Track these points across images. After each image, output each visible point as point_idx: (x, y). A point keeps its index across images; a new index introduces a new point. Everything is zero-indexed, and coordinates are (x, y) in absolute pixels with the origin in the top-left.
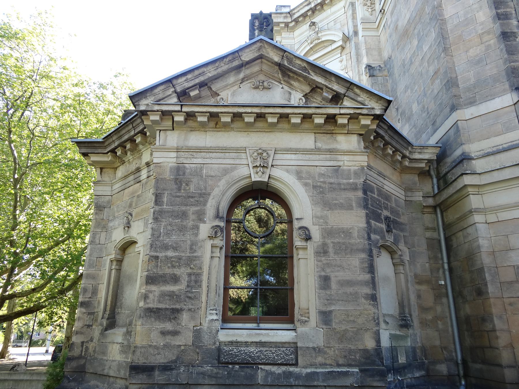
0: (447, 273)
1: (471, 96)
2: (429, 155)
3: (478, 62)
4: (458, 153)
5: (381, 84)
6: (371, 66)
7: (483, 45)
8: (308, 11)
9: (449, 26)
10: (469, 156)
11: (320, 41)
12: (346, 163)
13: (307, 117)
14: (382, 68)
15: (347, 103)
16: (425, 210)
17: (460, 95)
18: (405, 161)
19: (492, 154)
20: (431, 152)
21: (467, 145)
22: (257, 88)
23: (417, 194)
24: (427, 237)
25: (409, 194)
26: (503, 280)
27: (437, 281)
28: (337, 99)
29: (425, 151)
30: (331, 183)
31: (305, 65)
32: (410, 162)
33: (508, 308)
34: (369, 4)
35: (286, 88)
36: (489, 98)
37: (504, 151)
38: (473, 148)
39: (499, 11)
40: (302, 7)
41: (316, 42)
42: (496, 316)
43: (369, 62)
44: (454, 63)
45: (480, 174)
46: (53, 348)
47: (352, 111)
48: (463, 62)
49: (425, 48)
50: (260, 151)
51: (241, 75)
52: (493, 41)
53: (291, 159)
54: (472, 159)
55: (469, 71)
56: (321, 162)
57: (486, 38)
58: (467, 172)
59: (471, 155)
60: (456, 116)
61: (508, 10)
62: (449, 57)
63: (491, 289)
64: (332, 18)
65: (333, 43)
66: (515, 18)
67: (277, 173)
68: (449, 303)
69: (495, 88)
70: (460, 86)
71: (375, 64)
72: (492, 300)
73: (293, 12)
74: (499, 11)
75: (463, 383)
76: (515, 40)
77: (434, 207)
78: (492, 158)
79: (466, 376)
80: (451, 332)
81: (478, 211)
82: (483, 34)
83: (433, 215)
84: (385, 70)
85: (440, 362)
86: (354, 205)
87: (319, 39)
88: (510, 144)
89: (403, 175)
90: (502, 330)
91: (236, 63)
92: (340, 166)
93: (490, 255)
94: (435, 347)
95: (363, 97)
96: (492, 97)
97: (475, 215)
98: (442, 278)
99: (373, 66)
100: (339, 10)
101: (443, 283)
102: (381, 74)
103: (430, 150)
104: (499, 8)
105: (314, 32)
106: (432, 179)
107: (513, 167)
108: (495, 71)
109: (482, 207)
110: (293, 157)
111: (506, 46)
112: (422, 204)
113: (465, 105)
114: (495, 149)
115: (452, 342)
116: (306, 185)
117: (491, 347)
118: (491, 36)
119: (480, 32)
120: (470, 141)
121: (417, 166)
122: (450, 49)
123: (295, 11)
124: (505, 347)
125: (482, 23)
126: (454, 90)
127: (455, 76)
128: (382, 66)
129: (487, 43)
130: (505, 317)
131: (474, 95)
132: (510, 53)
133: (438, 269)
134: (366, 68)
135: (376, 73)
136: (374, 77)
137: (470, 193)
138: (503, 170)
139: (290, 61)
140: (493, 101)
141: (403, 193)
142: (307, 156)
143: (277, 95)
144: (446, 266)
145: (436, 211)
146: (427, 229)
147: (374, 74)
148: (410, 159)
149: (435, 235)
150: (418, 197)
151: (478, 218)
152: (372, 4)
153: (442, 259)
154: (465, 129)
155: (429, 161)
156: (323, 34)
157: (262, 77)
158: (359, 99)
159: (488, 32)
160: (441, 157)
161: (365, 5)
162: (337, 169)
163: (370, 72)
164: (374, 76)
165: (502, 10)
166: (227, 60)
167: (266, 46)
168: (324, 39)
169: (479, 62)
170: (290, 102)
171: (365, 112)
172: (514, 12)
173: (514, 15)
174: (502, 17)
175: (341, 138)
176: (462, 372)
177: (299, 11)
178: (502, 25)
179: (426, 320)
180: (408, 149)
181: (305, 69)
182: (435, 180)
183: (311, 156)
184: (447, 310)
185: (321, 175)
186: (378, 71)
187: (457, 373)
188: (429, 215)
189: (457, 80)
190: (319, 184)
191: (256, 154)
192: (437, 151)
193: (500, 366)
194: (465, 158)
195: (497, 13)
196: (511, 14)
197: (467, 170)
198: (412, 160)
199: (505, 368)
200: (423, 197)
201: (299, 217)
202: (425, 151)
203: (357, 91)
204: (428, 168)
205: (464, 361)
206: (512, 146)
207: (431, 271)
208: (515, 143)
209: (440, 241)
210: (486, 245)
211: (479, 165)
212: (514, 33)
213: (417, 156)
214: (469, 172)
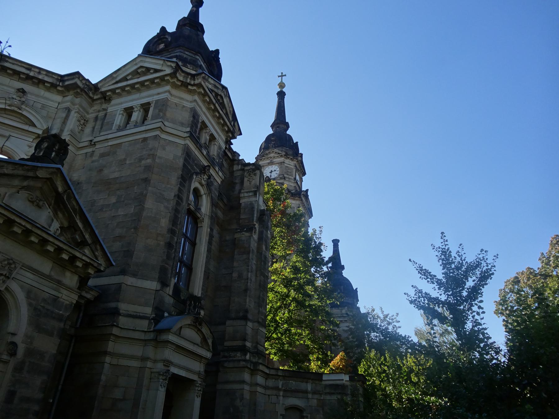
4: (113, 305)
8: (24, 73)
9: (144, 214)
11: (20, 111)
12: (64, 297)
13: (59, 250)
15: (87, 251)
22: (32, 202)
28: (82, 244)
30: (48, 310)
31: (77, 207)
34: (82, 123)
35: (51, 214)
38: (123, 307)
40: (20, 64)
41: (16, 109)
45: (121, 328)
47: (88, 261)
49: (121, 212)
50: (11, 262)
51: (25, 183)
53: (29, 278)
56: (48, 289)
64: (43, 101)
65: (32, 126)
67: (14, 286)
73: (7, 59)
81: (112, 354)
86: (55, 333)
87: (20, 109)
91: (30, 174)
92: (59, 297)
95: (99, 253)
96: (144, 277)
100: (52, 101)
105: (19, 99)
110: (32, 276)
114: (135, 314)
116: (30, 305)
123: (10, 61)
139: (69, 198)
142: (41, 280)
143: (43, 216)
152: (84, 124)
156: (27, 108)
157: (38, 193)
158: (97, 253)
161: (79, 121)
162: (56, 299)
166: (27, 168)
167: (59, 175)
168: (24, 113)
170: (50, 227)
171: (96, 265)
175: (68, 274)
177: (13, 64)
181: (75, 210)
182: (81, 315)
183: (43, 281)
185: (44, 300)
190: (39, 307)
191: (6, 262)
192: (96, 294)
194: (116, 312)
201: (12, 331)
203: (98, 247)
211: (122, 321)
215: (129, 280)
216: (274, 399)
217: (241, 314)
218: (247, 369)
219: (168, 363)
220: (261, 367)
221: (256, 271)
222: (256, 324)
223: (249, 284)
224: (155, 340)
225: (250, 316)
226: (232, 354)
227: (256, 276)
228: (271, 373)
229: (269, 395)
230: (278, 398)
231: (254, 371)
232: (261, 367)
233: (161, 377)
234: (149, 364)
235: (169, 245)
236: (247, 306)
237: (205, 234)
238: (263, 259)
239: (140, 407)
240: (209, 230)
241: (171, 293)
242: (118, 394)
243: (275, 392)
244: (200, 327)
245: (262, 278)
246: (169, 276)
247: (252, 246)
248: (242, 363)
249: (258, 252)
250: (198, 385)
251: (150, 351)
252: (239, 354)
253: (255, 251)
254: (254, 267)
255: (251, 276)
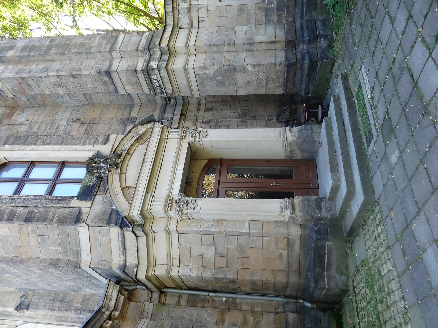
0: (217, 294)
1: (72, 252)
2: (114, 291)
3: (43, 241)
5: (40, 299)
6: (18, 306)
7: (30, 235)
10: (122, 266)
14: (24, 295)
16: (162, 301)
17: (68, 260)
18: (114, 315)
19: (125, 250)
20: (112, 289)
21: (113, 264)
23: (147, 306)
24: (185, 305)
25: (145, 315)
26: (224, 265)
27: (223, 304)
29: (110, 294)
32: (117, 310)
33: (245, 266)
36: (77, 240)
37: (124, 242)
39: (5, 218)
42: (252, 277)
43: (14, 306)
44: (37, 258)
45: (139, 263)
46: (255, 239)
48: (39, 251)
49: (17, 271)
52: (29, 227)
54: (125, 264)
55: (49, 249)
57: (25, 231)
58: (135, 271)
59: (121, 264)
60: (85, 266)
61: (7, 211)
62: (30, 260)
63: (231, 276)
66: (17, 208)
68: (241, 298)
69: (70, 235)
70: (60, 258)
71: (17, 301)
72: (239, 278)
74: (5, 218)
75: (301, 301)
76: (36, 213)
77: (161, 292)
78: (128, 251)
79: (296, 298)
80: (264, 301)
81: (169, 271)
82: (20, 232)
83: (168, 295)
84: (27, 293)
85: (286, 318)
88: (120, 237)
89: (127, 317)
90: (262, 275)
93: (204, 270)
94: (275, 320)
97: (172, 275)
98: (221, 298)
99: (18, 303)
101: (224, 299)
102: (30, 298)
103: (110, 290)
104: (3, 217)
106: (136, 289)
107: (138, 241)
108: (56, 232)
109: (166, 266)
111: (37, 221)
112: (156, 304)
113: (78, 258)
114: (121, 247)
115: (271, 302)
117: (275, 284)
118: (24, 228)
119: (17, 234)
120: (110, 262)
121: (121, 304)
122: (24, 258)
124: (274, 276)
125: (11, 231)
126: (61, 264)
127: (49, 260)
128: (22, 294)
129: (30, 232)
130: (252, 270)
131: (71, 250)
132: (44, 220)
133: (213, 300)
134: (18, 311)
135: (26, 302)
136: (30, 305)
137: (153, 274)
138: (139, 248)
140: (81, 239)
141: (143, 320)
144: (211, 294)
145: (165, 292)
146: (178, 302)
147: (27, 304)
148: (113, 310)
149: (185, 297)
150: (149, 307)
151: (174, 273)
153: (205, 296)
154: (99, 263)
155: (120, 292)
159: (20, 229)
160: (118, 281)
163: (24, 309)
164: (29, 305)
165: (5, 216)
169: (44, 241)
172: (11, 208)
173: (14, 208)
174: (11, 218)
176: (293, 300)
178: (18, 220)
179: (254, 323)
180: (103, 313)
184: (246, 300)
186: (26, 300)
187: (294, 304)
188: (167, 298)
189: (54, 259)
193: (287, 283)
194: (123, 268)
195: (5, 221)
196: (12, 210)
197: (134, 271)
198: (115, 308)
199: (289, 280)
200: (150, 302)
202: (110, 294)
204: (126, 293)
205: (286, 297)
206: (121, 236)
207: (214, 307)
208: (120, 233)
209: (190, 295)
210: (197, 271)
211: (131, 260)
212: (29, 212)
213: (112, 303)
214: (136, 270)
215: (85, 257)
216: (203, 14)
217: (106, 78)
218: (169, 67)
219: (169, 203)
220: (164, 44)
221: (46, 61)
222: (115, 54)
223: (63, 73)
224: (142, 226)
225: (104, 68)
226: (156, 84)
227: (53, 60)
228: (172, 23)
229: (199, 21)
230: (201, 8)
231: (171, 53)
232: (164, 44)
233: (185, 212)
234: (172, 227)
235: (28, 219)
236: (93, 72)
237: (13, 152)
238: (26, 53)
239: (219, 230)
240: (7, 147)
241: (89, 204)
242: (209, 253)
243: (194, 14)
244: (124, 153)
245: (53, 51)
246: (68, 210)
247: (11, 75)
248: (164, 73)
249: (20, 62)
250: (193, 141)
251: (158, 227)
252: (154, 77)
253: (19, 67)
254: (41, 66)
255: (53, 71)
